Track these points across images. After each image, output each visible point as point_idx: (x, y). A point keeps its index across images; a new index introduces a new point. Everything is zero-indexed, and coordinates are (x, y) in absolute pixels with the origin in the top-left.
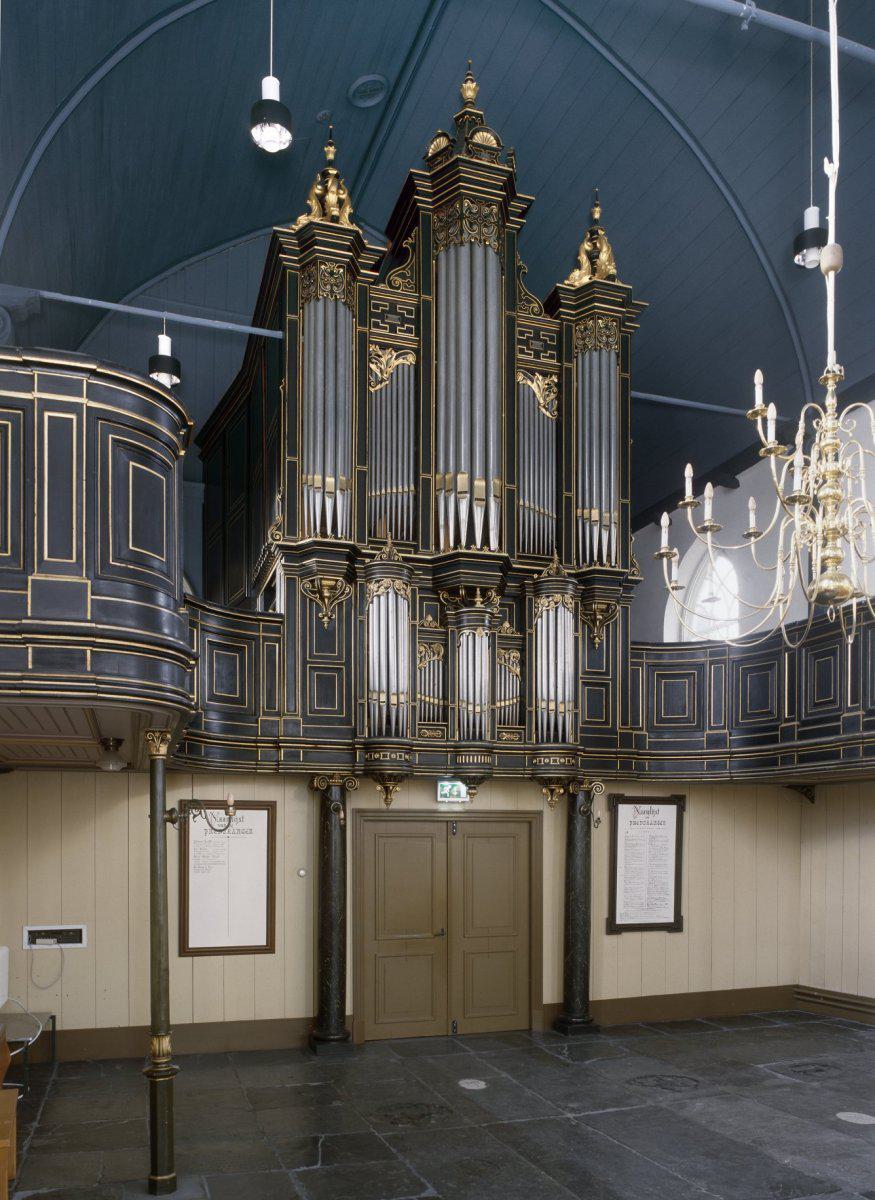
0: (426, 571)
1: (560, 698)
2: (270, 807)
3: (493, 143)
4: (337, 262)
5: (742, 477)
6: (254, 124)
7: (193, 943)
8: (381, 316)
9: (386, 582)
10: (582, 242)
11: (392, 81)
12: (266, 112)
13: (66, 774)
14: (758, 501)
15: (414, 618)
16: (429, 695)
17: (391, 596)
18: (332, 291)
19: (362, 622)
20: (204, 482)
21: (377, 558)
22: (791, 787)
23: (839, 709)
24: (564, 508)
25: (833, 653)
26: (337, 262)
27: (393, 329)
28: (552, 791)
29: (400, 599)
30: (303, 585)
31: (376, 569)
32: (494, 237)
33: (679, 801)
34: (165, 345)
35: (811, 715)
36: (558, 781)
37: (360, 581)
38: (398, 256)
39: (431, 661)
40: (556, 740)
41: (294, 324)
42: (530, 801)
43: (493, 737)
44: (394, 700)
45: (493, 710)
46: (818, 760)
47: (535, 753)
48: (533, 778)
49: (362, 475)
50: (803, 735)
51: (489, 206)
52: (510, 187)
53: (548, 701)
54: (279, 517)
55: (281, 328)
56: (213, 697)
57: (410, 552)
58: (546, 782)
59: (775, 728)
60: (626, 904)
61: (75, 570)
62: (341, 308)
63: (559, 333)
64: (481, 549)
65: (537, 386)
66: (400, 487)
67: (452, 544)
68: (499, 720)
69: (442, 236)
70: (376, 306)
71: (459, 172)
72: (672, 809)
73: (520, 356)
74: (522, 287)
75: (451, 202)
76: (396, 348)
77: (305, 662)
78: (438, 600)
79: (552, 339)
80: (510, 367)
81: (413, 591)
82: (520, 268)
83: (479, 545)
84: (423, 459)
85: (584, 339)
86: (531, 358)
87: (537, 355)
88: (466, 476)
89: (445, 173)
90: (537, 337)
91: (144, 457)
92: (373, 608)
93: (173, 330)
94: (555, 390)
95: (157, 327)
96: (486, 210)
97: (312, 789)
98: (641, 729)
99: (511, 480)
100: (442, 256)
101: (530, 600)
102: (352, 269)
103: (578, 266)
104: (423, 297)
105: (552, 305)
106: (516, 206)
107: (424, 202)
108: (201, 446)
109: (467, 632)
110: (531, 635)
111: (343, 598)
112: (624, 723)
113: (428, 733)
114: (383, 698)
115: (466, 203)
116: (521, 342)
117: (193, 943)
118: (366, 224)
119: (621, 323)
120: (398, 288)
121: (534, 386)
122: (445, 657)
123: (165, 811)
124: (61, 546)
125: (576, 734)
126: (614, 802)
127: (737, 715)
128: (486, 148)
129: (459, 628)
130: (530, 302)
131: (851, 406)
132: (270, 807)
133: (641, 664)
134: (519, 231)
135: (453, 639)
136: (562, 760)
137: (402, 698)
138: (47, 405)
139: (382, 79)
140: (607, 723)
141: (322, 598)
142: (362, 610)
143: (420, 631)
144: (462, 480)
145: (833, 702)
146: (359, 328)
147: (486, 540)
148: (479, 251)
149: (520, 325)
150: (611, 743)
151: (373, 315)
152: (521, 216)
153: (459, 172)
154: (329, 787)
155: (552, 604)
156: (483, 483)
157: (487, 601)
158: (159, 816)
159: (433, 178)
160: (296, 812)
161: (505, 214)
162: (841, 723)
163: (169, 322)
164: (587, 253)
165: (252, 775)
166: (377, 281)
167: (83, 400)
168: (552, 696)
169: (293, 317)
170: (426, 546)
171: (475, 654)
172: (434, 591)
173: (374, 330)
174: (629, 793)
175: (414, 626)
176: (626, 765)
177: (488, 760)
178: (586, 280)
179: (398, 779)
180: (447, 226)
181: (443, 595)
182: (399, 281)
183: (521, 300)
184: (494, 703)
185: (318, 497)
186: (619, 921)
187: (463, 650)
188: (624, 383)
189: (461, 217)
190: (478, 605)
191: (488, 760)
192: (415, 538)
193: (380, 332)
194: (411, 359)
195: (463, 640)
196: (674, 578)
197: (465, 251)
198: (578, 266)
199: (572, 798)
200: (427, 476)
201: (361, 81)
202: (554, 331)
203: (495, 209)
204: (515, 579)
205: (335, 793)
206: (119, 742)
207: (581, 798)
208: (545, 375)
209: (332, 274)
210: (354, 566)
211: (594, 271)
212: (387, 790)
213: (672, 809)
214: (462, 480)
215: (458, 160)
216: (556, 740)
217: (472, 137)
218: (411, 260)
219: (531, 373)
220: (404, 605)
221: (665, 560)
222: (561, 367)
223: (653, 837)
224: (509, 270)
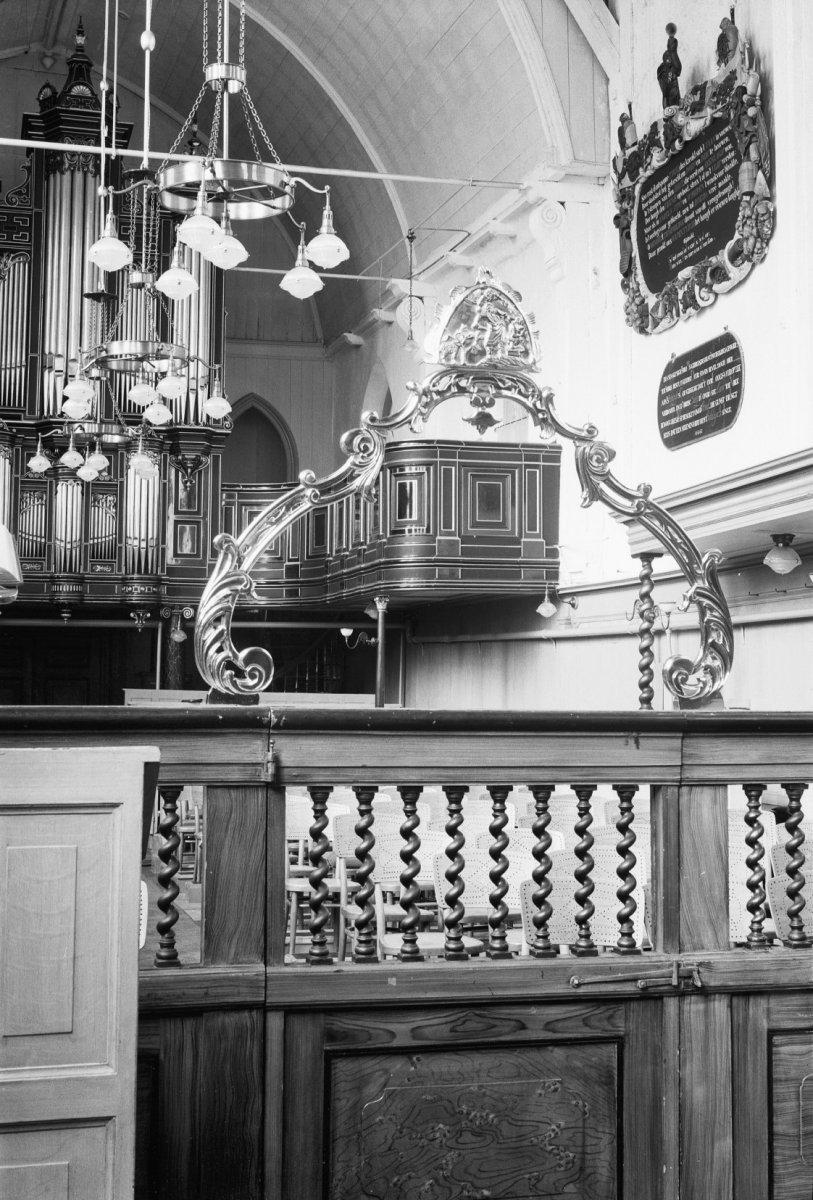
16: (45, 537)
22: (506, 694)
43: (85, 568)
45: (86, 547)
57: (19, 418)
66: (563, 841)
79: (24, 222)
101: (122, 454)
120: (15, 203)
129: (57, 480)
133: (453, 464)
136: (143, 589)
143: (22, 482)
162: (436, 544)
175: (17, 479)
177: (80, 588)
184: (86, 540)
191: (80, 588)
192: (25, 405)
197: (67, 176)
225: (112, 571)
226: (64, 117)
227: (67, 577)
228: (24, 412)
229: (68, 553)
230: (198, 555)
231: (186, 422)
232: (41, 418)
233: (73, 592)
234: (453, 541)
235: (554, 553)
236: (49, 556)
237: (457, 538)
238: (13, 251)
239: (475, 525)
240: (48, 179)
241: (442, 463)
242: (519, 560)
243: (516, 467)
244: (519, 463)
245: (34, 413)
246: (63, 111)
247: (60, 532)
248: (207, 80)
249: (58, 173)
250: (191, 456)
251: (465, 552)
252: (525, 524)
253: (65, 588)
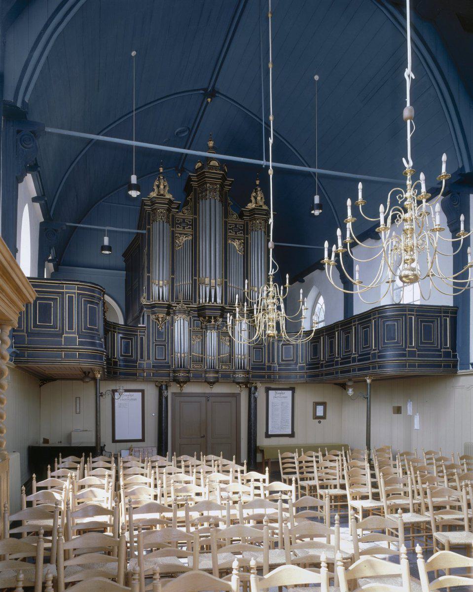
0: (194, 311)
1: (242, 354)
2: (143, 391)
3: (217, 164)
4: (163, 209)
6: (129, 191)
7: (117, 438)
8: (180, 224)
9: (180, 316)
10: (252, 193)
12: (133, 187)
13: (74, 381)
17: (182, 321)
18: (161, 218)
19: (172, 329)
21: (178, 308)
23: (371, 350)
25: (368, 327)
26: (163, 209)
27: (184, 228)
28: (240, 386)
30: (153, 317)
31: (177, 311)
32: (218, 196)
33: (293, 389)
34: (106, 241)
35: (363, 352)
36: (242, 383)
38: (186, 203)
39: (197, 341)
40: (241, 369)
41: (149, 229)
42: (235, 389)
43: (219, 368)
44: (183, 355)
46: (345, 373)
47: (234, 373)
48: (234, 382)
49: (173, 279)
53: (238, 355)
56: (122, 356)
57: (190, 304)
58: (238, 383)
59: (319, 364)
60: (272, 427)
61: (74, 333)
62: (165, 224)
64: (213, 303)
65: (236, 244)
67: (204, 302)
68: (221, 361)
69: (200, 195)
70: (178, 221)
71: (205, 175)
72: (290, 392)
73: (230, 234)
74: (230, 209)
75: (204, 184)
76: (185, 234)
77: (153, 343)
80: (226, 239)
81: (191, 318)
82: (229, 204)
84: (195, 271)
85: (252, 227)
86: (234, 234)
88: (208, 279)
89: (201, 176)
90: (236, 227)
91: (91, 302)
92: (176, 324)
93: (110, 234)
94: (243, 245)
95: (103, 233)
96: (215, 187)
99: (226, 278)
100: (201, 202)
103: (251, 201)
107: (194, 184)
109: (209, 331)
111: (166, 321)
112: (269, 361)
113: (196, 367)
114: (179, 355)
115: (208, 185)
116: (230, 229)
117: (117, 438)
121: (235, 244)
122: (202, 340)
124: (71, 327)
125: (249, 365)
126: (268, 390)
128: (214, 166)
130: (233, 215)
132: (143, 391)
134: (229, 191)
135: (204, 334)
138: (67, 293)
140: (262, 362)
141: (159, 321)
142: (172, 325)
144: (207, 280)
146: (172, 229)
147: (215, 300)
148: (213, 201)
149: (229, 223)
150: (264, 369)
153: (205, 175)
154: (162, 385)
156: (214, 281)
160: (152, 392)
163: (108, 231)
164: (254, 197)
165: (135, 380)
166: (177, 212)
167: (76, 291)
168: (240, 353)
169: (149, 227)
171: (212, 337)
173: (177, 229)
174: (273, 386)
175: (190, 330)
176: (269, 377)
177: (216, 375)
179: (185, 382)
180: (202, 192)
183: (230, 214)
185: (157, 287)
186: (270, 433)
187: (208, 336)
189: (206, 190)
191: (216, 375)
192: (192, 300)
193: (180, 230)
194: (190, 238)
195: (208, 334)
197: (208, 201)
198: (251, 201)
200: (196, 278)
201: (178, 130)
202: (243, 224)
205: (164, 387)
207: (253, 389)
209: (161, 212)
210: (169, 310)
211: (256, 203)
212: (181, 387)
213: (290, 392)
214: (207, 280)
215: (204, 172)
216: (241, 369)
218: (191, 204)
219: (233, 239)
220: (186, 323)
223: (282, 402)
225: (229, 368)
226: (207, 175)
227: (183, 370)
229: (213, 361)
233: (215, 377)
236: (204, 362)
239: (422, 343)
241: (444, 316)
242: (350, 365)
244: (78, 292)
245: (150, 300)
246: (207, 172)
247: (237, 350)
248: (440, 197)
250: (161, 316)
252: (443, 344)
253: (212, 375)
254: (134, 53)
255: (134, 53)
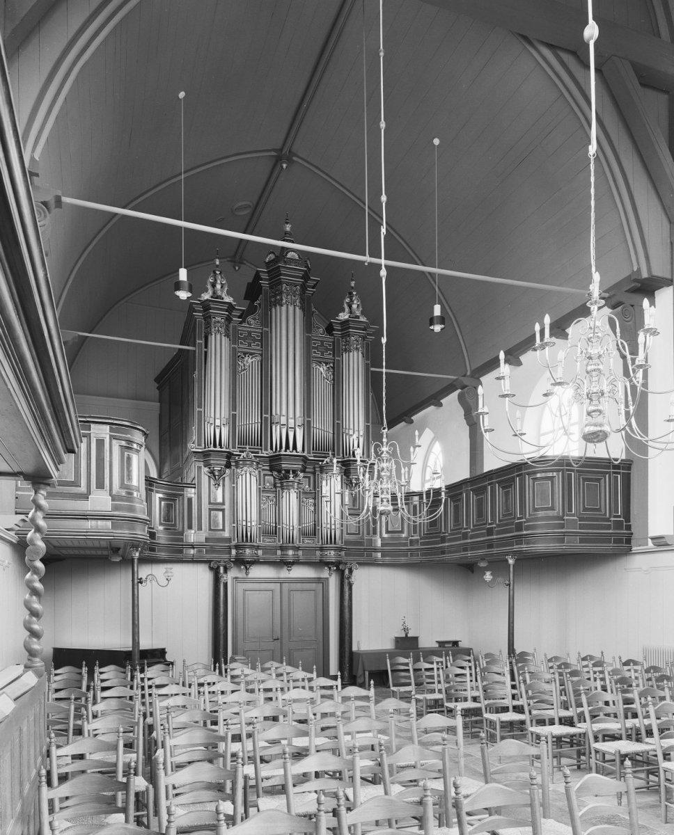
5: (522, 358)
8: (244, 339)
10: (345, 299)
11: (255, 203)
14: (419, 432)
15: (260, 485)
20: (159, 402)
24: (338, 428)
27: (250, 345)
28: (330, 568)
29: (252, 476)
35: (476, 526)
36: (332, 563)
37: (233, 468)
38: (251, 310)
42: (325, 573)
44: (249, 524)
50: (499, 533)
51: (295, 286)
52: (306, 277)
53: (327, 524)
54: (195, 438)
55: (194, 346)
62: (223, 338)
63: (334, 343)
67: (278, 449)
68: (303, 533)
78: (272, 475)
79: (330, 345)
82: (313, 312)
83: (291, 449)
87: (322, 354)
97: (211, 569)
98: (619, 517)
102: (229, 319)
104: (264, 329)
105: (330, 329)
106: (310, 283)
108: (158, 383)
110: (318, 491)
118: (247, 261)
119: (364, 338)
121: (321, 369)
123: (138, 579)
127: (580, 510)
131: (575, 321)
133: (619, 473)
137: (253, 524)
139: (248, 203)
145: (484, 520)
151: (239, 338)
152: (313, 287)
155: (329, 477)
157: (296, 475)
158: (136, 581)
159: (268, 272)
161: (304, 287)
166: (241, 323)
170: (266, 450)
171: (291, 499)
172: (271, 470)
173: (240, 346)
178: (347, 317)
181: (275, 473)
182: (252, 322)
187: (284, 499)
188: (367, 364)
190: (291, 478)
192: (261, 445)
195: (284, 494)
196: (485, 425)
199: (343, 572)
203: (298, 287)
204: (311, 464)
206: (119, 549)
207: (347, 572)
208: (326, 364)
212: (246, 567)
217: (286, 255)
218: (259, 311)
221: (481, 416)
222: (334, 360)
224: (307, 315)
228: (261, 449)
229: (249, 529)
230: (359, 534)
231: (215, 446)
232: (276, 452)
233: (534, 543)
234: (573, 519)
235: (629, 527)
237: (576, 518)
238: (251, 354)
240: (271, 309)
243: (607, 473)
249: (278, 307)
251: (581, 527)
254: (182, 95)
255: (182, 95)
